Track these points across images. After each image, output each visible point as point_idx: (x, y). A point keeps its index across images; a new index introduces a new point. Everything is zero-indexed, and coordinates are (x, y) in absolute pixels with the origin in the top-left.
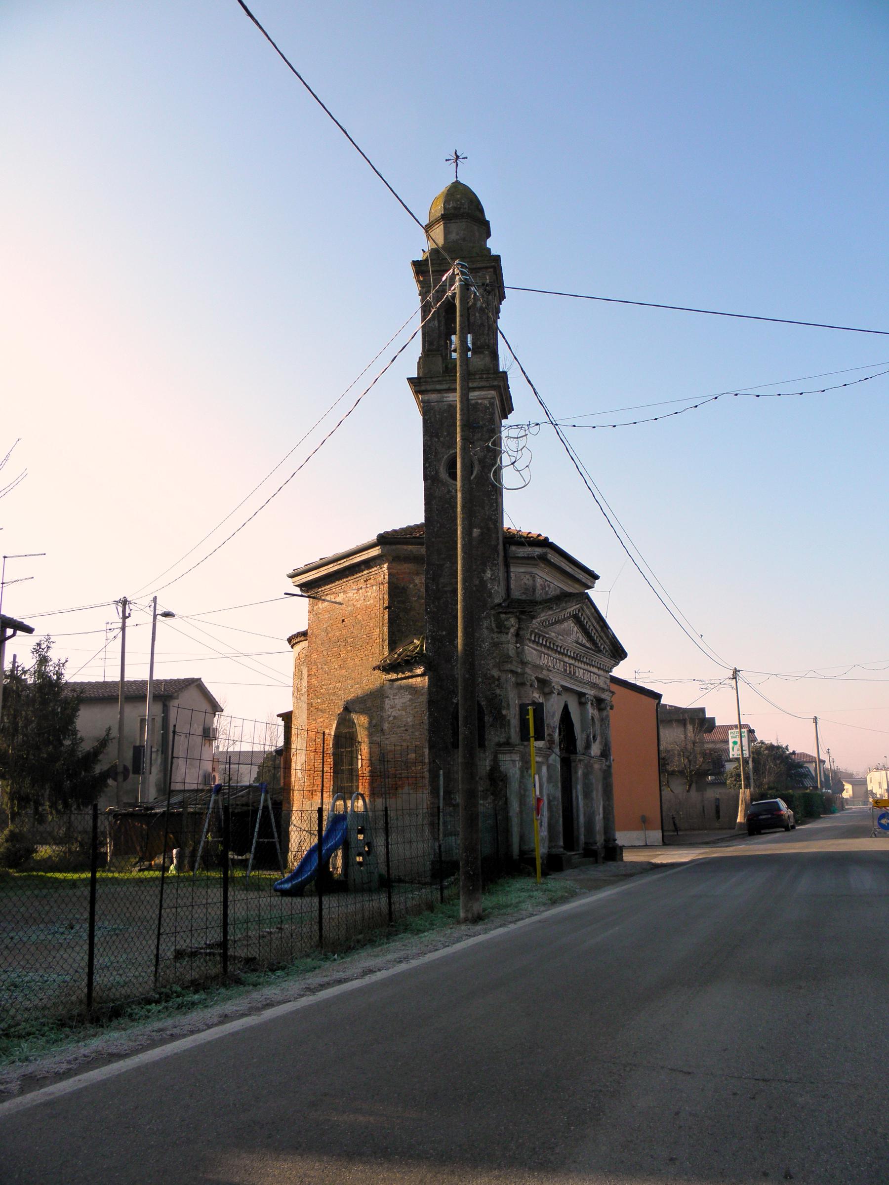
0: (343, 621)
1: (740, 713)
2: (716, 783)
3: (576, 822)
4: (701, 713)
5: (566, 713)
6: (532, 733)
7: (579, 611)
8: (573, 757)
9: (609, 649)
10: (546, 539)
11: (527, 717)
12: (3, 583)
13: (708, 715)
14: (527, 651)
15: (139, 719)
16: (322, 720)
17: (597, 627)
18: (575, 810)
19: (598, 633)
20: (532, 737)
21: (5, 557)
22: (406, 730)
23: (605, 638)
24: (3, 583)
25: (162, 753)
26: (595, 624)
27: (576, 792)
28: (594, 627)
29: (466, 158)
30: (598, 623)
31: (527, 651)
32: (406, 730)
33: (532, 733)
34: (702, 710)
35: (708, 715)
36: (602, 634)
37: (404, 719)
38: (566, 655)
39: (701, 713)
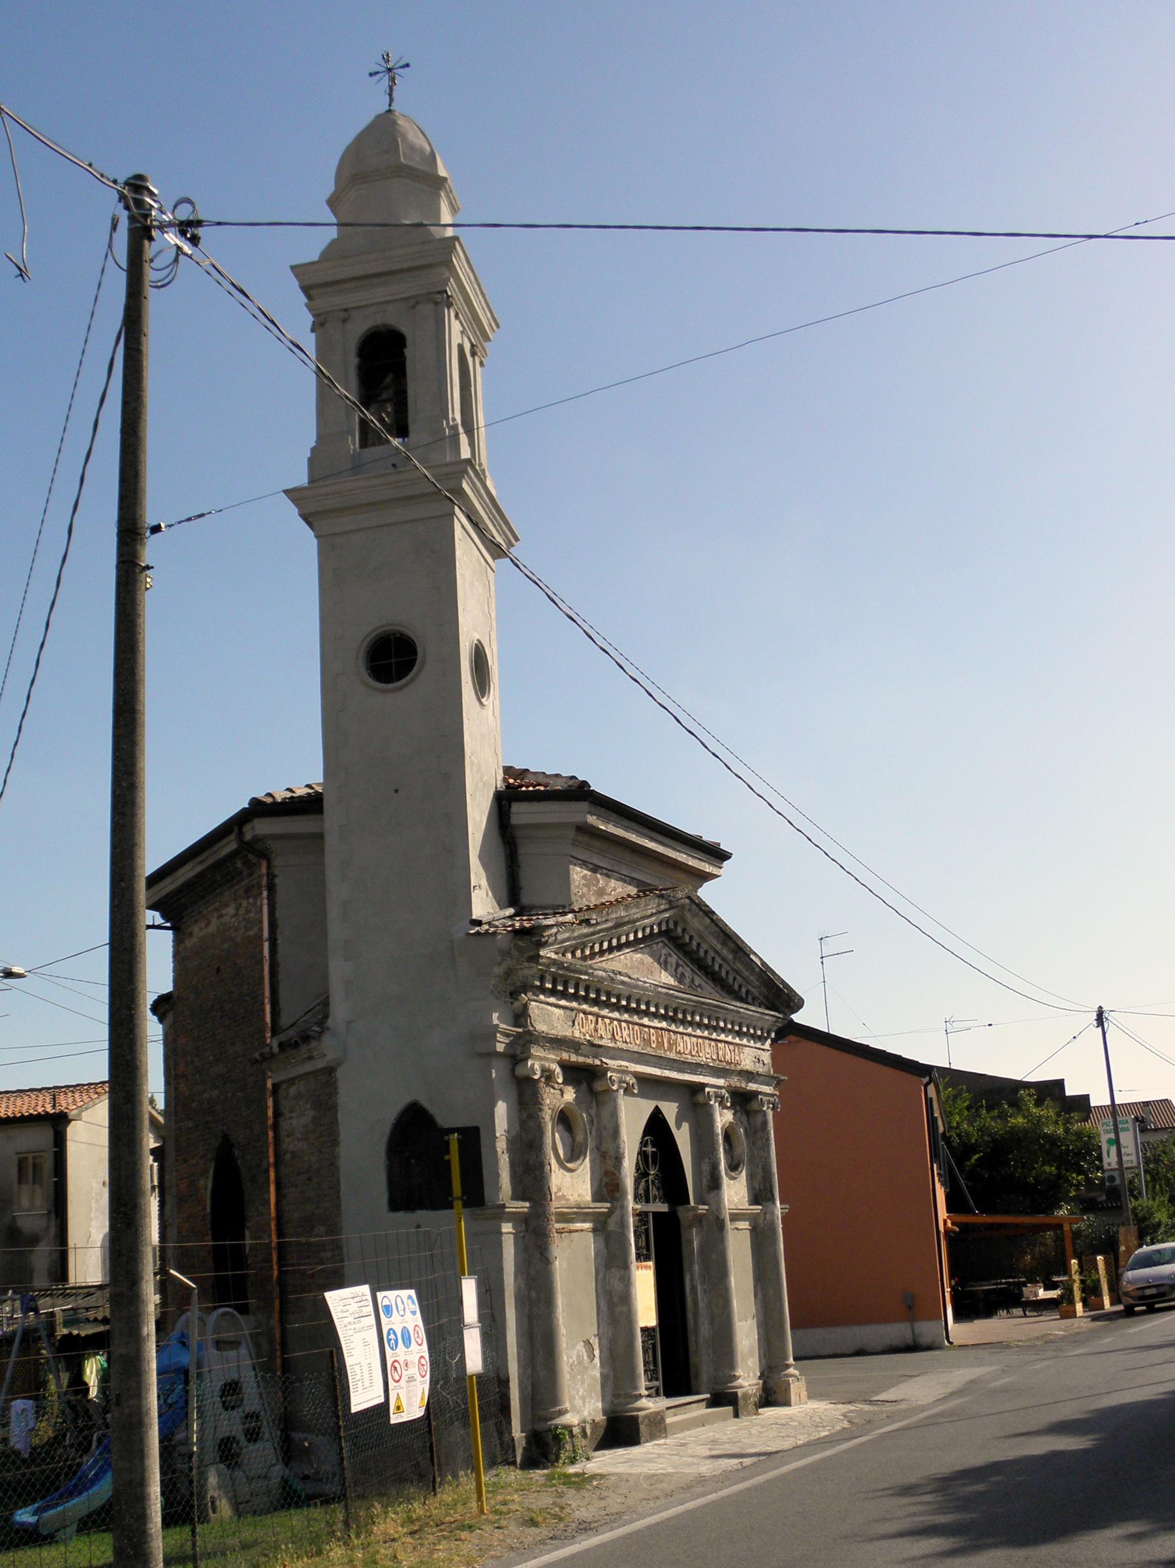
0: (218, 970)
1: (1114, 1089)
2: (1109, 1207)
3: (693, 1338)
4: (1057, 1089)
5: (656, 1127)
6: (457, 1189)
7: (676, 924)
8: (681, 1210)
9: (760, 993)
10: (585, 784)
11: (447, 1157)
12: (822, 958)
13: (1070, 1091)
14: (537, 1012)
15: (16, 1158)
16: (194, 1162)
17: (725, 952)
18: (690, 1316)
19: (728, 963)
20: (458, 1198)
21: (822, 939)
22: (309, 1179)
23: (746, 973)
24: (822, 958)
25: (57, 1218)
26: (719, 947)
27: (692, 1279)
28: (716, 952)
29: (371, 75)
30: (724, 944)
31: (537, 1012)
32: (309, 1179)
33: (457, 1189)
34: (1059, 1084)
35: (1070, 1091)
36: (739, 966)
37: (306, 1159)
38: (646, 1013)
39: (1057, 1089)
